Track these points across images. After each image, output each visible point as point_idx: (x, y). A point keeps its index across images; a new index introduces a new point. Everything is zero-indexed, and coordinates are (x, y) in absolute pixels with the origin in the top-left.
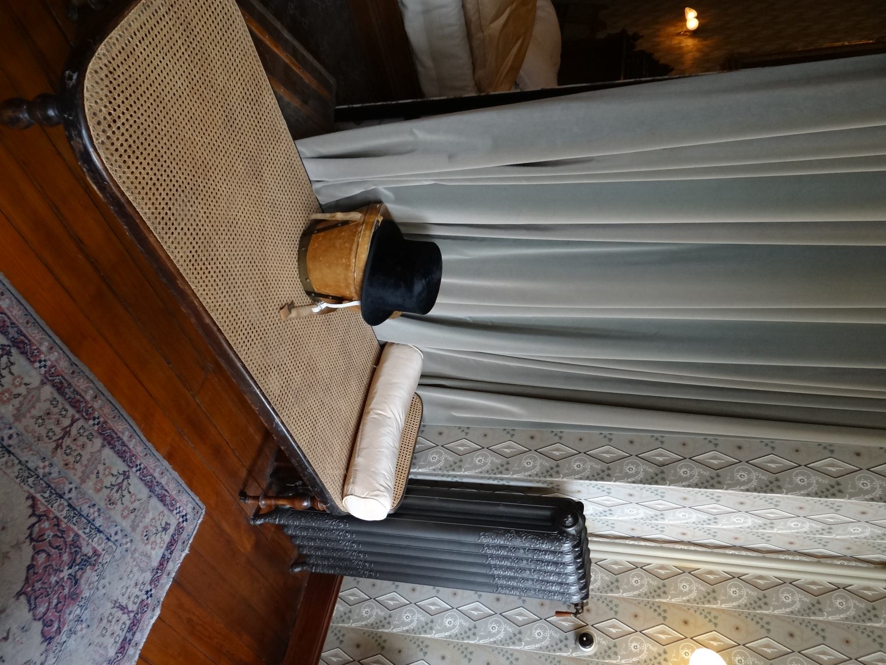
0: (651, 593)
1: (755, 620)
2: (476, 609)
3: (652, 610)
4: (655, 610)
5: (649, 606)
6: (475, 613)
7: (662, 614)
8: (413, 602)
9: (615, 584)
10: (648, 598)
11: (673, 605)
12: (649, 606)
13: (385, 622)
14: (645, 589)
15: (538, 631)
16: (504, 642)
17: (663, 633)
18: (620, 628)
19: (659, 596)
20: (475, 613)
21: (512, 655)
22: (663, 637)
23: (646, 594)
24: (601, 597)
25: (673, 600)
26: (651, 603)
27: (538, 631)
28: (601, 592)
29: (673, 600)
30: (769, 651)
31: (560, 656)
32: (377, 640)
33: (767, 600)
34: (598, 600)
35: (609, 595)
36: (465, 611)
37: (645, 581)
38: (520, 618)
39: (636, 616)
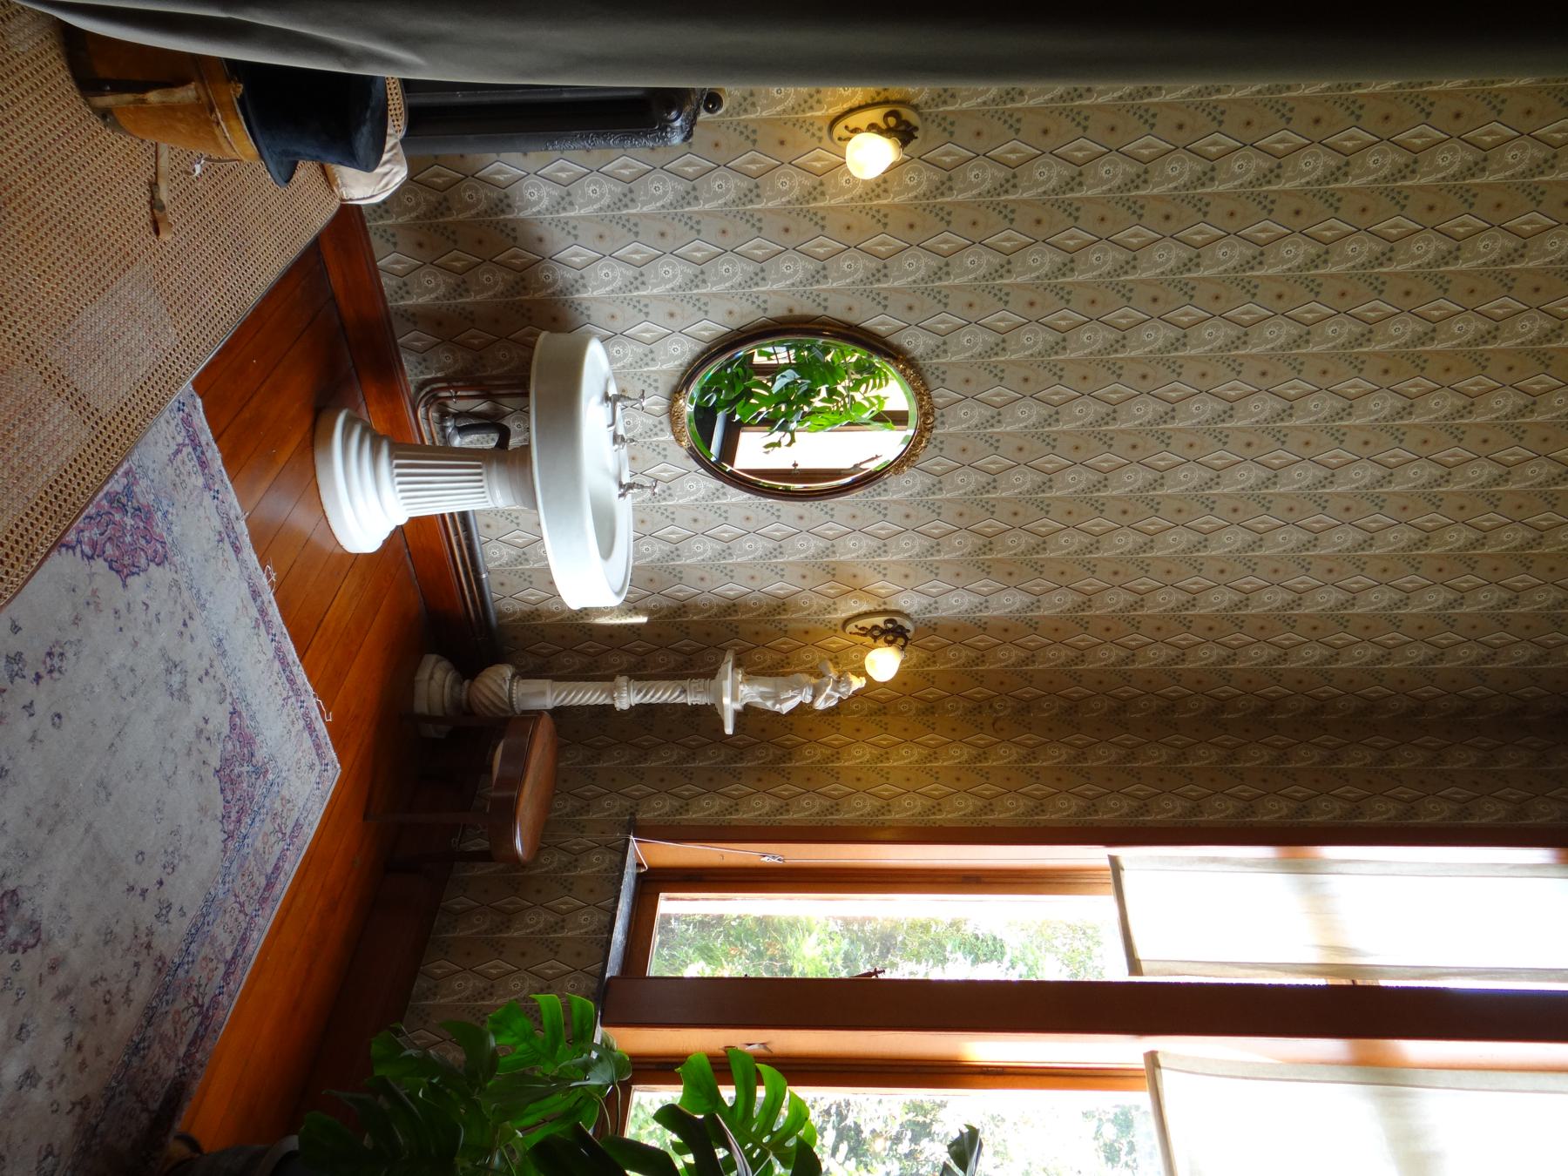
0: (740, 199)
1: (808, 216)
2: (882, 244)
3: (620, 225)
4: (624, 226)
5: (615, 221)
6: (882, 249)
7: (633, 228)
8: (607, 253)
9: (693, 194)
10: (737, 206)
11: (645, 215)
12: (615, 221)
13: (1515, 255)
14: (606, 200)
15: (724, 267)
16: (805, 282)
17: (636, 252)
18: (952, 243)
19: (626, 206)
20: (882, 249)
21: (878, 294)
22: (637, 257)
23: (609, 206)
24: (676, 214)
25: (645, 209)
26: (741, 212)
27: (724, 267)
28: (801, 204)
29: (645, 209)
30: (399, 267)
31: (639, 296)
32: (814, 301)
33: (633, 196)
34: (673, 219)
35: (686, 209)
36: (1380, 231)
37: (606, 188)
38: (821, 250)
39: (601, 237)
